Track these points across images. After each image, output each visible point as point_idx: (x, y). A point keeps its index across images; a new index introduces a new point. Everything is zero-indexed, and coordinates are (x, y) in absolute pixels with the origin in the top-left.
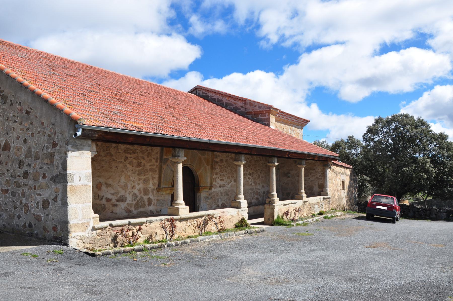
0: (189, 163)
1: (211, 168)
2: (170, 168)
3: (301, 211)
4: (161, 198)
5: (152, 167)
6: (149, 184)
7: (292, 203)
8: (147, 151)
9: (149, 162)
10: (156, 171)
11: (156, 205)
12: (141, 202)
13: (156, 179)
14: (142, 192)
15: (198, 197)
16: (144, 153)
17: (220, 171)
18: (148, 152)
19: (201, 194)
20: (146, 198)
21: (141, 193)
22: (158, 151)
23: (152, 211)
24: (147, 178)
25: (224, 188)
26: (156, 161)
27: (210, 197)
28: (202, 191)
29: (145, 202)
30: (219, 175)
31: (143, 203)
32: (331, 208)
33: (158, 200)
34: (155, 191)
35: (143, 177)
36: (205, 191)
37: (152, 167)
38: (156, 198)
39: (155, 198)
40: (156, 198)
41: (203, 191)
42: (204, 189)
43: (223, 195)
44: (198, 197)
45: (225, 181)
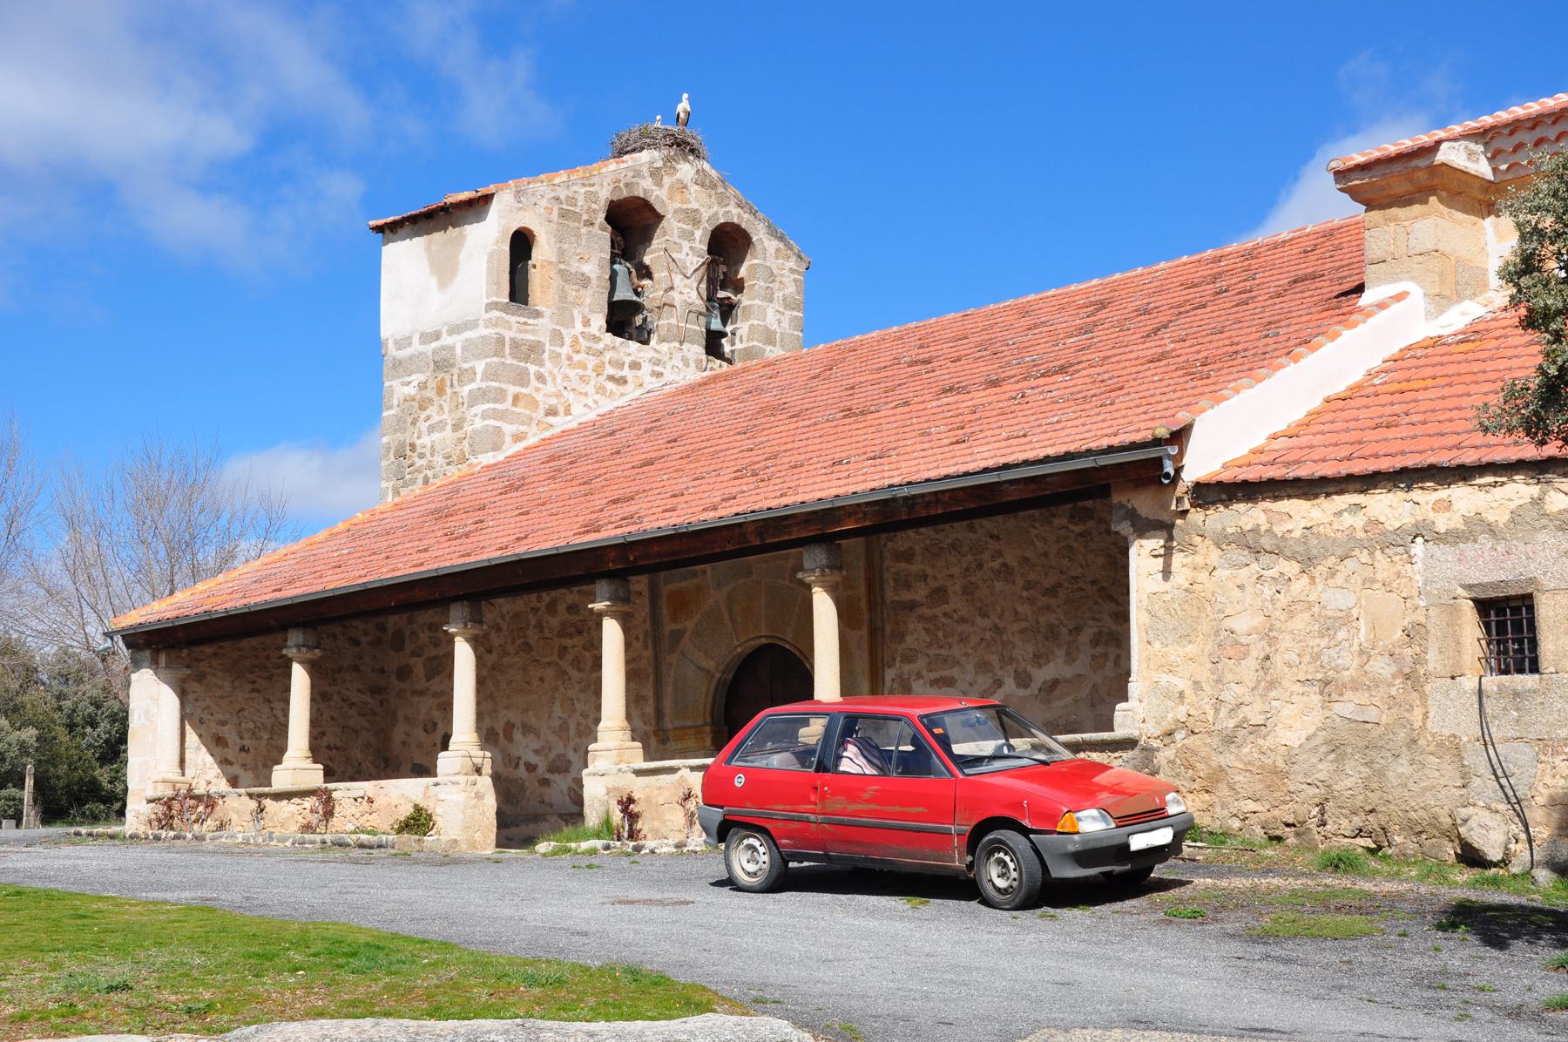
0: (764, 633)
17: (930, 645)
30: (921, 663)
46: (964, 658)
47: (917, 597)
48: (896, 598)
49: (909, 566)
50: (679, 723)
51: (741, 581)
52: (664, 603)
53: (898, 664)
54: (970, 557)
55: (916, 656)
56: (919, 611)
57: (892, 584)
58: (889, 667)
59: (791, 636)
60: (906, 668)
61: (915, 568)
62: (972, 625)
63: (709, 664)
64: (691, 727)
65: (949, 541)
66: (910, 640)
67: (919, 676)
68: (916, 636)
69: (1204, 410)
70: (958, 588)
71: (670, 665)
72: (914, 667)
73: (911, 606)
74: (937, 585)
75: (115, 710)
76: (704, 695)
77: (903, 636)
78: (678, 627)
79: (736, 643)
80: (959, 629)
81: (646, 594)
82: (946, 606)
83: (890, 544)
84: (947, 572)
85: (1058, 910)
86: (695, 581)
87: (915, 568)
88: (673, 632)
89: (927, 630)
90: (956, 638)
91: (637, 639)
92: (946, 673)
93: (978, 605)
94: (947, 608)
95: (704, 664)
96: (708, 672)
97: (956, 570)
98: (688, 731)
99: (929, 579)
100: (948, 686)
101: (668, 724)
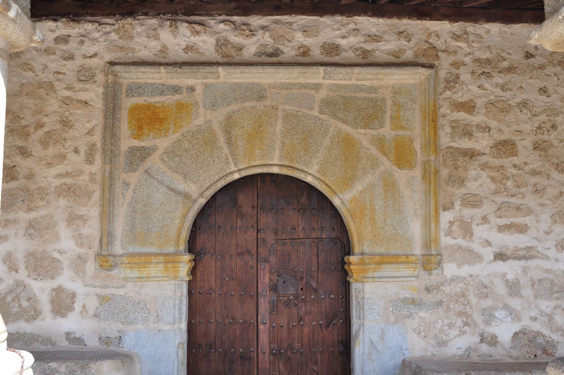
0: (276, 161)
1: (424, 178)
2: (162, 183)
3: (416, 365)
4: (122, 292)
5: (69, 181)
6: (57, 238)
7: (409, 271)
8: (42, 126)
9: (49, 165)
10: (89, 194)
11: (96, 316)
12: (17, 298)
13: (90, 223)
14: (22, 266)
15: (357, 298)
16: (28, 134)
17: (496, 192)
18: (46, 129)
19: (367, 286)
20: (42, 290)
21: (17, 271)
22: (95, 122)
23: (77, 336)
24: (42, 217)
25: (532, 263)
26: (90, 160)
27: (429, 298)
28: (370, 274)
29: (37, 301)
30: (487, 208)
31: (25, 304)
32: (465, 66)
33: (103, 299)
34: (91, 266)
35: (23, 216)
36: (383, 274)
37: (69, 181)
38: (98, 290)
39: (92, 289)
40: (98, 290)
41: (376, 274)
42: (380, 263)
43: (527, 292)
44: (357, 298)
45: (532, 232)
46: (539, 208)
47: (478, 147)
48: (454, 144)
49: (469, 117)
50: (132, 249)
51: (247, 104)
52: (124, 116)
53: (457, 207)
54: (543, 117)
55: (481, 201)
56: (483, 159)
57: (449, 130)
58: (445, 209)
59: (316, 167)
60: (468, 212)
61: (477, 119)
62: (548, 178)
63: (193, 189)
64: (157, 255)
65: (517, 100)
66: (472, 186)
67: (485, 220)
68: (479, 182)
69: (427, 64)
70: (528, 142)
71: (127, 184)
72: (478, 212)
73: (471, 154)
74: (503, 137)
75: (457, 85)
76: (177, 221)
77: (463, 181)
78: (143, 144)
79: (233, 168)
80: (534, 180)
81: (99, 104)
82: (515, 158)
83: (448, 92)
84: (515, 127)
85: (353, 288)
86: (177, 97)
87: (477, 119)
88: (133, 151)
89: (493, 179)
90: (530, 188)
91: (76, 151)
92: (519, 220)
93: (556, 161)
94: (516, 160)
95: (182, 186)
96: (187, 196)
97: (527, 127)
98: (154, 260)
99: (492, 131)
100: (520, 232)
101: (118, 249)
